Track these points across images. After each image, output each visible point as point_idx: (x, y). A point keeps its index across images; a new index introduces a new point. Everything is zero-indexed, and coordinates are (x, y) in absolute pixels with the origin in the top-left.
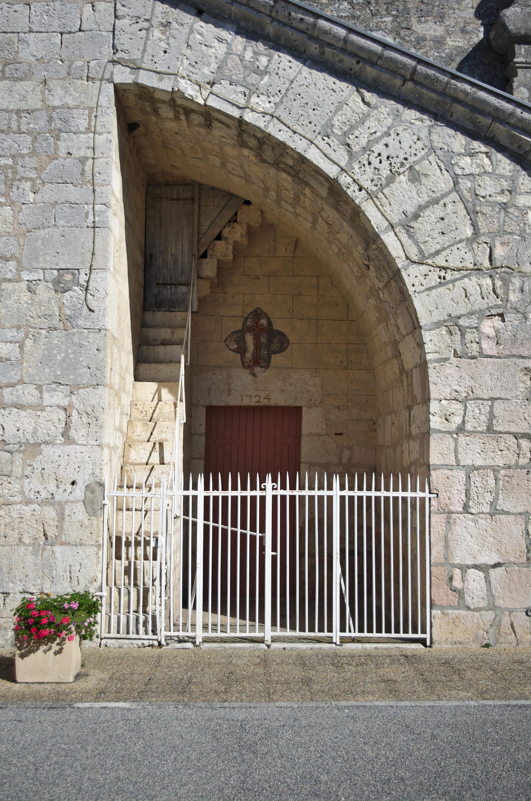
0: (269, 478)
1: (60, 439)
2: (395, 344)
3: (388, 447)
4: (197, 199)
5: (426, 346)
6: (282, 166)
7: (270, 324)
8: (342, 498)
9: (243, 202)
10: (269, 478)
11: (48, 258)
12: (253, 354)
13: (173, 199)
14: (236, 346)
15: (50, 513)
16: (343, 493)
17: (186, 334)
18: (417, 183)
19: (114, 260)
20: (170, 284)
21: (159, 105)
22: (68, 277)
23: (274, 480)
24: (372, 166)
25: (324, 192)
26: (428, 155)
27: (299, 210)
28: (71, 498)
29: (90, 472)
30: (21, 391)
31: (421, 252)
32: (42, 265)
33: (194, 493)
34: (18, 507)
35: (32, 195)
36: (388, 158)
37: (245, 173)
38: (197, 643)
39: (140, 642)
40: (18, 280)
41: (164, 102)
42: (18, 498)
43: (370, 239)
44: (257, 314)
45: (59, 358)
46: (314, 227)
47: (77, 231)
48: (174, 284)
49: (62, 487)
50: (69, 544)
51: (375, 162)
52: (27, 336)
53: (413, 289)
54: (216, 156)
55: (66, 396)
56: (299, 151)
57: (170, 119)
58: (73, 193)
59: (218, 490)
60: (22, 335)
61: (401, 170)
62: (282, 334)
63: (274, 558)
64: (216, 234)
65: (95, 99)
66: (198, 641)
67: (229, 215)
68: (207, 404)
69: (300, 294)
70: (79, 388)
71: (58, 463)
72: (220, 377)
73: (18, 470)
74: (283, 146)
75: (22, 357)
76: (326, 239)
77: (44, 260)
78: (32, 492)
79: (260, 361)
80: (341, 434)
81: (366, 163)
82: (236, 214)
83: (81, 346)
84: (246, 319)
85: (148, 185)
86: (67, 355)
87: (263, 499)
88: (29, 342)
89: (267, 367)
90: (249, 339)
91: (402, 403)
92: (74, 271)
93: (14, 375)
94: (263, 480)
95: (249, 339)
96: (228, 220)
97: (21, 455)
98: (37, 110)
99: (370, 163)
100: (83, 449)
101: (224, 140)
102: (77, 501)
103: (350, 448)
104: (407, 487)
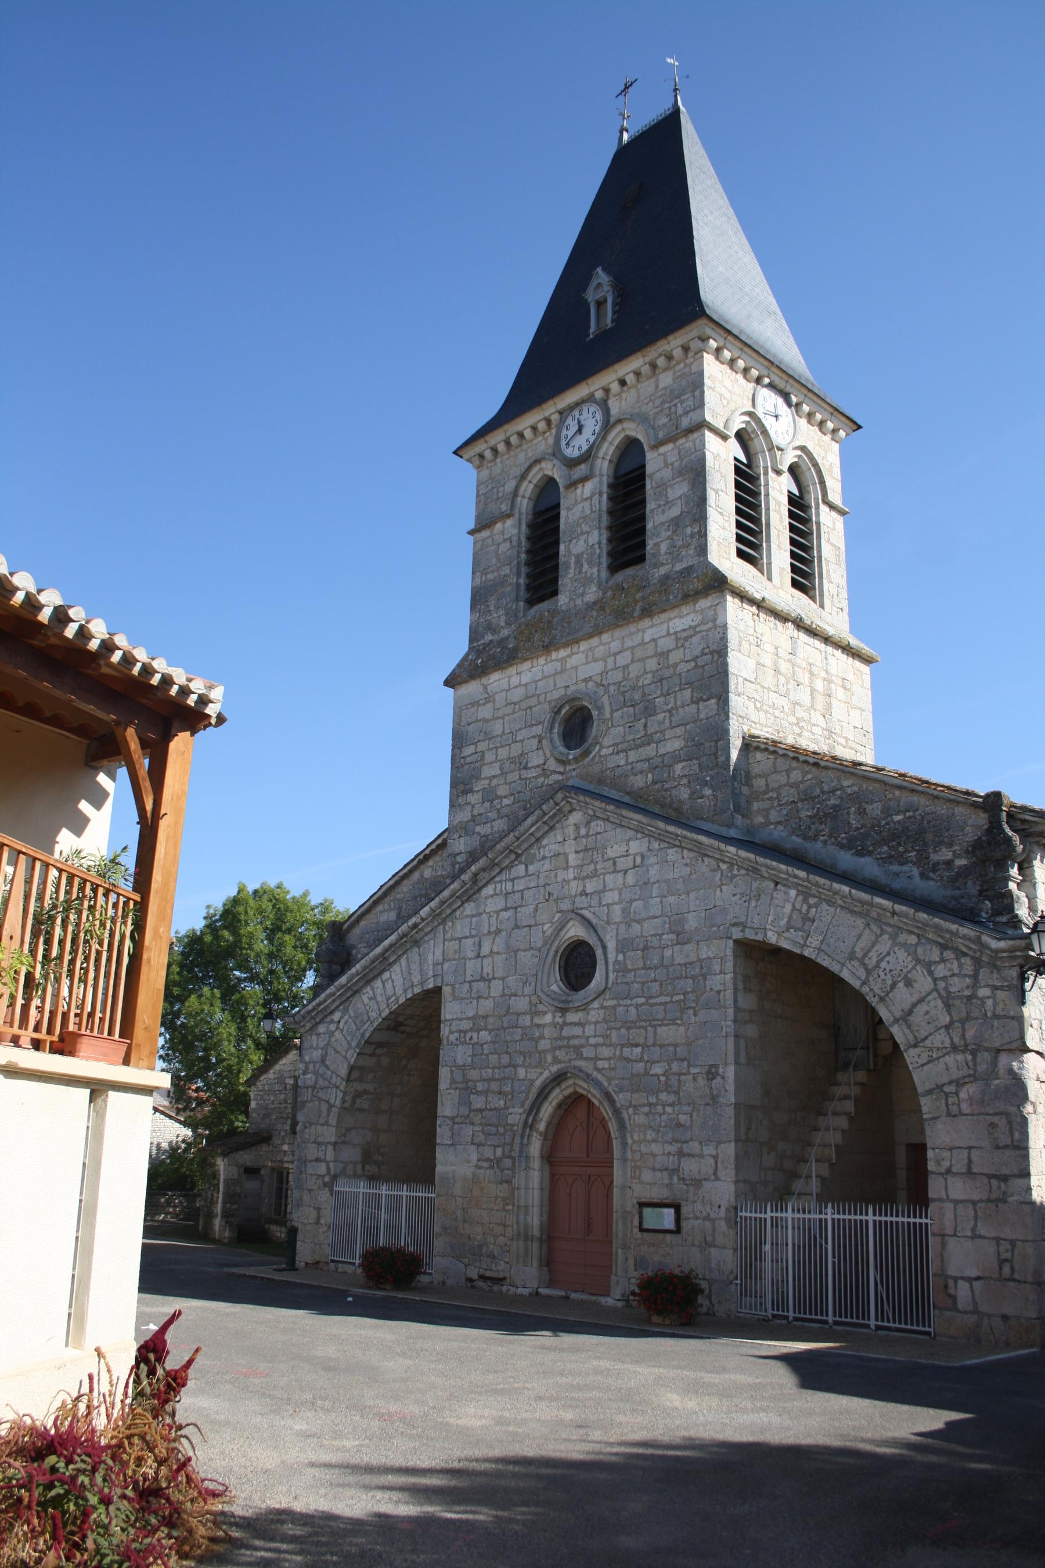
0: (830, 1206)
1: (713, 1177)
10: (830, 1206)
23: (833, 1208)
26: (916, 965)
31: (915, 1037)
40: (688, 1073)
51: (882, 974)
63: (834, 1262)
66: (791, 1319)
73: (691, 1196)
83: (721, 1115)
88: (695, 1114)
92: (716, 1066)
94: (826, 1208)
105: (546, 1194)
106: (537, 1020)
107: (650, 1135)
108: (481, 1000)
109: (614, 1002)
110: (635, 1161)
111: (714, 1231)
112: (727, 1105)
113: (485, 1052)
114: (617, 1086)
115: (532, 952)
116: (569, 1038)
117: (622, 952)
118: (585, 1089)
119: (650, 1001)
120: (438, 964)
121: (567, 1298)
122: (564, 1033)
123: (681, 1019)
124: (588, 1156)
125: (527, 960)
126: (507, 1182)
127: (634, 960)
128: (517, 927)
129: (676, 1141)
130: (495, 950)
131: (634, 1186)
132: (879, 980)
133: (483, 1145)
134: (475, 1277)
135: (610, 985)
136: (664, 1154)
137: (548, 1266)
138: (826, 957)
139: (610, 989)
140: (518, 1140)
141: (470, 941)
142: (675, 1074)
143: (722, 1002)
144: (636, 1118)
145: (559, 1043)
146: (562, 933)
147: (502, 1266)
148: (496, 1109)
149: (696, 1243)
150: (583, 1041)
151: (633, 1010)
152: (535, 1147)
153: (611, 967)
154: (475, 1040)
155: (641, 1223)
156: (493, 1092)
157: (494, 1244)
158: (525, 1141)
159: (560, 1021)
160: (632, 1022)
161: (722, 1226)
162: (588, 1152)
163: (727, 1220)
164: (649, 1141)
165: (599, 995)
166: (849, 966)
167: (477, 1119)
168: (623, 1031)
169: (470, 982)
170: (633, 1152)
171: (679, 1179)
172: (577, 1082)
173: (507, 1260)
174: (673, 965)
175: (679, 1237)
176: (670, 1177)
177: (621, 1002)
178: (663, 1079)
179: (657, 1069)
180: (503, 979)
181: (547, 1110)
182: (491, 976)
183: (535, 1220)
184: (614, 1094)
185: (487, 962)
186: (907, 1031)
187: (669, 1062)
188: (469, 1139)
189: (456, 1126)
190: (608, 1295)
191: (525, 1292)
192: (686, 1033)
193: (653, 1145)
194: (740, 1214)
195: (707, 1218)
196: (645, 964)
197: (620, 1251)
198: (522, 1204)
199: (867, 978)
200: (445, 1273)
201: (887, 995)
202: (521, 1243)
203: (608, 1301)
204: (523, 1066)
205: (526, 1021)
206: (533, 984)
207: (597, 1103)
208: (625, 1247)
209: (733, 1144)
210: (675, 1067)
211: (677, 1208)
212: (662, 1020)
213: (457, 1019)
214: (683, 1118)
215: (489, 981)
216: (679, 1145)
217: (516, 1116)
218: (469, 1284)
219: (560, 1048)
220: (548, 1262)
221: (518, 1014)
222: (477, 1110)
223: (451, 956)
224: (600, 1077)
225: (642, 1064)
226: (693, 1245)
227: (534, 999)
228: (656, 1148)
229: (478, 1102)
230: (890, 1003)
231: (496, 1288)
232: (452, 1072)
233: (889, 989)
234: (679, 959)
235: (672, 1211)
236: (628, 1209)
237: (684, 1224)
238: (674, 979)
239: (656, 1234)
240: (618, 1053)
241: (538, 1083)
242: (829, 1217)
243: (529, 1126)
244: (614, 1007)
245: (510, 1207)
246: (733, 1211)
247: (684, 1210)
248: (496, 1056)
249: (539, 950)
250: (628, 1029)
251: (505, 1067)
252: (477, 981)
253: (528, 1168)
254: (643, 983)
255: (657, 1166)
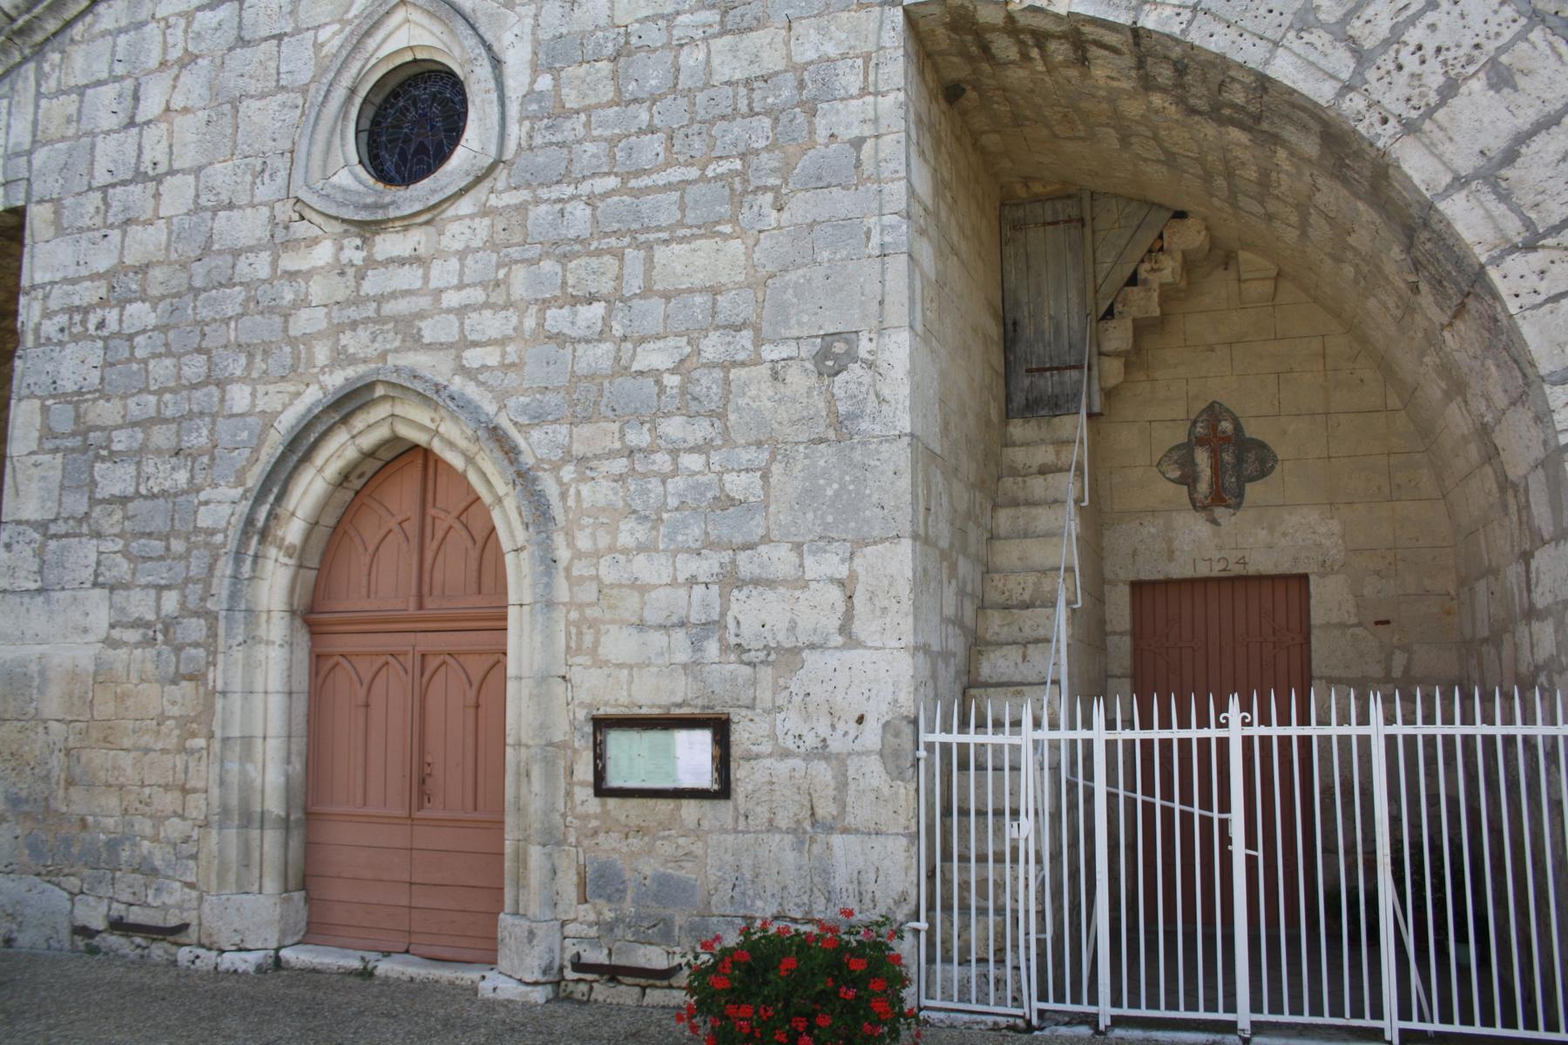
0: (1234, 704)
1: (839, 640)
2: (1484, 431)
3: (1485, 640)
4: (1088, 218)
5: (1556, 417)
6: (1227, 112)
7: (1238, 428)
8: (1391, 740)
9: (1170, 214)
10: (1234, 704)
11: (805, 318)
12: (1211, 486)
13: (1045, 224)
14: (1178, 473)
15: (823, 772)
16: (1391, 730)
17: (1078, 453)
18: (1506, 91)
19: (924, 315)
20: (1050, 369)
21: (988, 36)
22: (839, 347)
23: (1246, 706)
24: (1406, 71)
25: (1310, 147)
26: (1528, 29)
27: (1273, 206)
28: (857, 747)
29: (890, 698)
30: (766, 557)
31: (1528, 224)
32: (795, 332)
33: (1087, 734)
34: (767, 762)
35: (774, 213)
36: (1439, 50)
37: (1165, 151)
38: (1102, 1027)
39: (990, 1020)
40: (757, 361)
41: (994, 28)
42: (766, 748)
43: (1416, 225)
44: (1214, 412)
45: (830, 492)
46: (1304, 234)
47: (851, 265)
48: (1057, 369)
49: (841, 727)
50: (857, 831)
51: (1411, 63)
52: (773, 459)
53: (1518, 302)
54: (1108, 125)
55: (843, 561)
56: (1251, 65)
57: (1013, 62)
58: (842, 202)
59: (1133, 728)
60: (766, 455)
61: (1471, 69)
62: (1262, 446)
63: (1251, 862)
64: (1128, 273)
65: (872, 38)
66: (1104, 1021)
67: (1147, 239)
68: (1132, 577)
69: (1291, 371)
70: (867, 545)
71: (833, 683)
72: (1153, 530)
73: (765, 696)
74: (1220, 63)
75: (767, 495)
76: (1330, 255)
77: (799, 323)
78: (790, 738)
79: (1224, 496)
80: (1387, 622)
81: (1392, 66)
82: (1161, 237)
83: (865, 468)
84: (1194, 423)
85: (1002, 205)
86: (843, 486)
87: (1223, 743)
88: (776, 469)
89: (1238, 506)
90: (1202, 458)
91: (1508, 549)
92: (849, 337)
93: (756, 527)
94: (1222, 707)
95: (1202, 458)
96: (1145, 249)
97: (769, 670)
98: (776, 73)
99: (1400, 68)
100: (876, 655)
101: (1115, 84)
102: (867, 753)
103: (1406, 649)
104: (1534, 714)
105: (301, 705)
106: (288, 262)
107: (630, 532)
108: (134, 230)
109: (524, 195)
110: (581, 607)
111: (842, 785)
112: (886, 439)
113: (139, 354)
114: (524, 409)
115: (281, 97)
116: (380, 299)
117: (550, 69)
118: (423, 428)
119: (633, 183)
120: (18, 155)
121: (366, 974)
122: (370, 287)
123: (734, 220)
124: (421, 607)
125: (266, 118)
126: (191, 678)
127: (587, 83)
128: (242, 42)
129: (712, 545)
130: (178, 102)
131: (576, 674)
132: (1401, 79)
133: (126, 587)
134: (98, 923)
135: (508, 156)
136: (674, 583)
137: (304, 885)
138: (1219, 28)
139: (509, 164)
140: (225, 568)
141: (110, 91)
142: (712, 365)
143: (868, 168)
144: (585, 489)
145: (353, 313)
146: (371, 43)
147: (176, 894)
148: (164, 493)
149: (783, 822)
150: (424, 302)
151: (580, 212)
152: (274, 584)
153: (513, 110)
154: (112, 325)
155: (599, 775)
156: (159, 452)
157: (155, 839)
158: (246, 569)
159: (359, 257)
160: (577, 240)
161: (873, 773)
162: (420, 596)
163: (888, 756)
164: (626, 551)
165: (478, 180)
166: (1297, 46)
167: (110, 521)
168: (548, 266)
169: (104, 189)
170: (574, 582)
171: (725, 648)
172: (400, 410)
173: (191, 878)
174: (707, 85)
175: (723, 808)
176: (696, 646)
177: (544, 193)
178: (672, 381)
179: (654, 357)
180: (197, 171)
181: (310, 489)
182: (162, 169)
183: (271, 775)
184: (513, 432)
185: (151, 134)
186: (1500, 209)
187: (694, 336)
188: (87, 575)
189: (53, 544)
190: (492, 963)
191: (246, 962)
192: (748, 256)
193: (641, 560)
194: (924, 737)
195: (821, 751)
196: (619, 91)
197: (535, 854)
198: (235, 732)
199: (1359, 72)
200: (12, 916)
201: (1430, 112)
202: (232, 834)
203: (498, 985)
204: (242, 380)
205: (261, 265)
206: (283, 174)
207: (457, 461)
208: (552, 839)
209: (906, 546)
210: (713, 347)
211: (720, 728)
212: (671, 228)
213: (65, 280)
214: (737, 484)
215: (159, 179)
216: (726, 556)
217: (222, 507)
218: (81, 942)
219: (354, 325)
220: (306, 878)
221: (236, 253)
222: (112, 500)
223: (53, 132)
224: (471, 391)
225: (607, 347)
226: (771, 827)
227: (285, 211)
228: (645, 568)
229: (115, 479)
230: (1438, 135)
231: (158, 951)
232: (45, 410)
233: (1433, 99)
234: (727, 69)
235: (704, 738)
236: (558, 737)
237: (739, 772)
238: (711, 123)
239: (650, 802)
240: (530, 323)
241: (288, 420)
242: (1235, 734)
243: (257, 531)
244: (522, 208)
245: (200, 742)
246: (908, 730)
247: (740, 736)
248: (168, 362)
249: (304, 90)
250: (565, 258)
251: (194, 387)
252: (124, 183)
253: (251, 640)
254: (613, 142)
255: (652, 617)
